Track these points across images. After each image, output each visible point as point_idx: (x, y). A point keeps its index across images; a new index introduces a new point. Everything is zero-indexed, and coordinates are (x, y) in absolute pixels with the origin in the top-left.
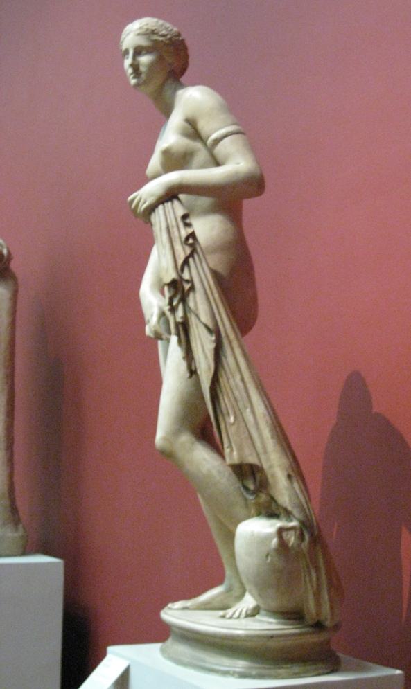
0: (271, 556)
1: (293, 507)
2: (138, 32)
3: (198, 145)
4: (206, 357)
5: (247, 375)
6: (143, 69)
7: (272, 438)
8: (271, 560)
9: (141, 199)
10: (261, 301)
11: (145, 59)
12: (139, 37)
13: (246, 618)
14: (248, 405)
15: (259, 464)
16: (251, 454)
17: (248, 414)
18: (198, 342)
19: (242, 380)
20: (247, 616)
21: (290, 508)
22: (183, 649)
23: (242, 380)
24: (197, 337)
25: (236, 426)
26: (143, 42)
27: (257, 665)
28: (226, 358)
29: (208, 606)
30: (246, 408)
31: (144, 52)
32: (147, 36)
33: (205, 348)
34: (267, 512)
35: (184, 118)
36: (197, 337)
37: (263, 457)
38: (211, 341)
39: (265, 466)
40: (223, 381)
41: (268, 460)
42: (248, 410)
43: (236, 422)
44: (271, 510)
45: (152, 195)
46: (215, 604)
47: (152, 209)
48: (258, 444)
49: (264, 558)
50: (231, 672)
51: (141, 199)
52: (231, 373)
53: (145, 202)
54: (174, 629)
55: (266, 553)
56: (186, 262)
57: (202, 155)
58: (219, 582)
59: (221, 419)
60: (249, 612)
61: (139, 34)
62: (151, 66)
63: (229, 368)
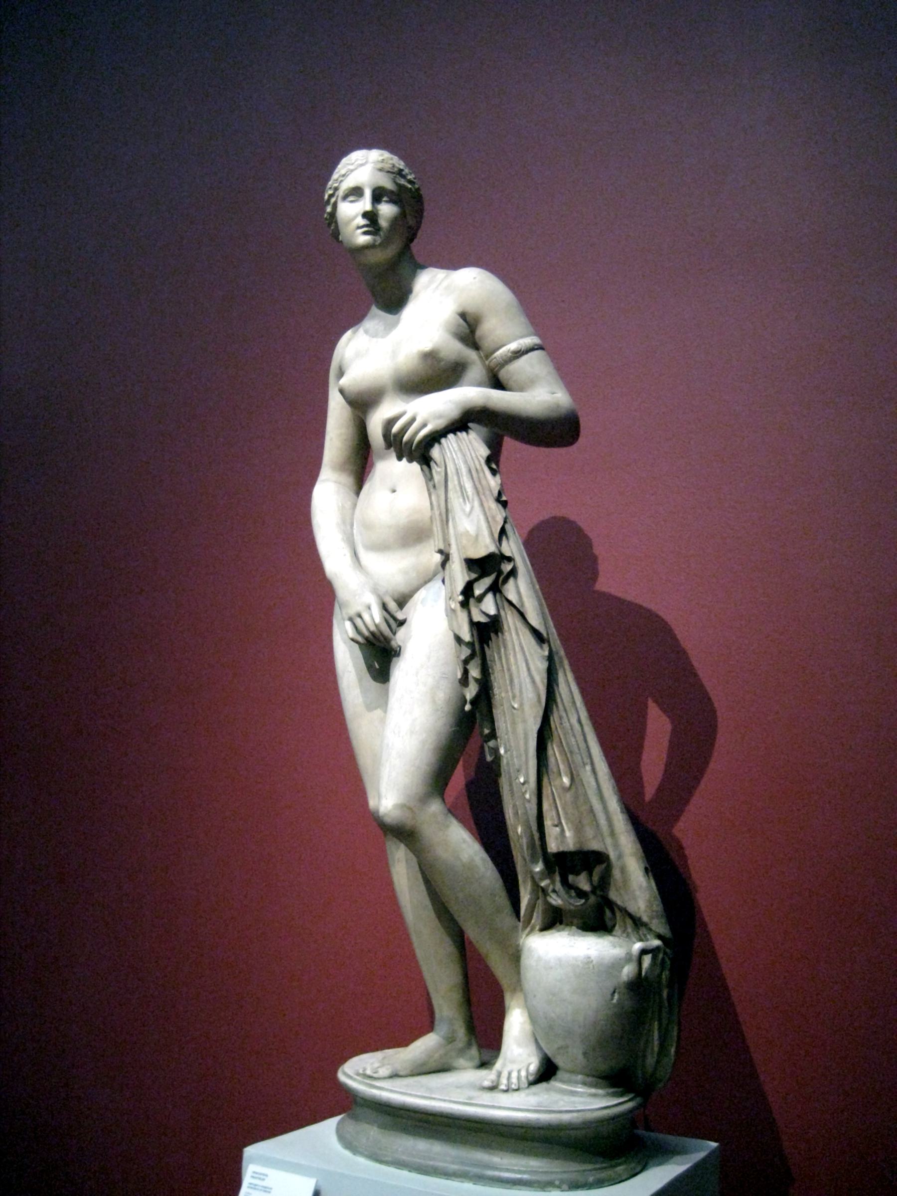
0: (619, 993)
1: (652, 918)
2: (380, 166)
3: (472, 355)
4: (533, 682)
5: (584, 714)
6: (383, 223)
7: (622, 812)
8: (619, 999)
9: (413, 420)
10: (652, 607)
11: (387, 210)
12: (380, 173)
13: (506, 1088)
14: (587, 760)
15: (605, 851)
16: (594, 838)
17: (586, 774)
18: (519, 656)
19: (579, 721)
20: (532, 1083)
21: (645, 919)
22: (371, 1133)
23: (579, 721)
24: (517, 648)
25: (573, 790)
26: (387, 183)
27: (590, 1167)
28: (558, 685)
29: (424, 1069)
30: (584, 764)
31: (385, 199)
32: (392, 176)
33: (532, 667)
34: (584, 923)
35: (460, 310)
36: (517, 648)
37: (609, 841)
38: (543, 657)
39: (612, 855)
40: (554, 720)
41: (616, 845)
42: (588, 768)
43: (573, 787)
44: (598, 918)
45: (440, 417)
46: (432, 1065)
47: (435, 437)
48: (603, 821)
49: (609, 996)
50: (557, 1183)
51: (413, 420)
52: (565, 710)
53: (424, 425)
54: (358, 1099)
55: (612, 990)
56: (503, 532)
57: (476, 371)
58: (429, 1026)
59: (545, 781)
60: (531, 1078)
61: (381, 170)
62: (395, 222)
63: (562, 700)
